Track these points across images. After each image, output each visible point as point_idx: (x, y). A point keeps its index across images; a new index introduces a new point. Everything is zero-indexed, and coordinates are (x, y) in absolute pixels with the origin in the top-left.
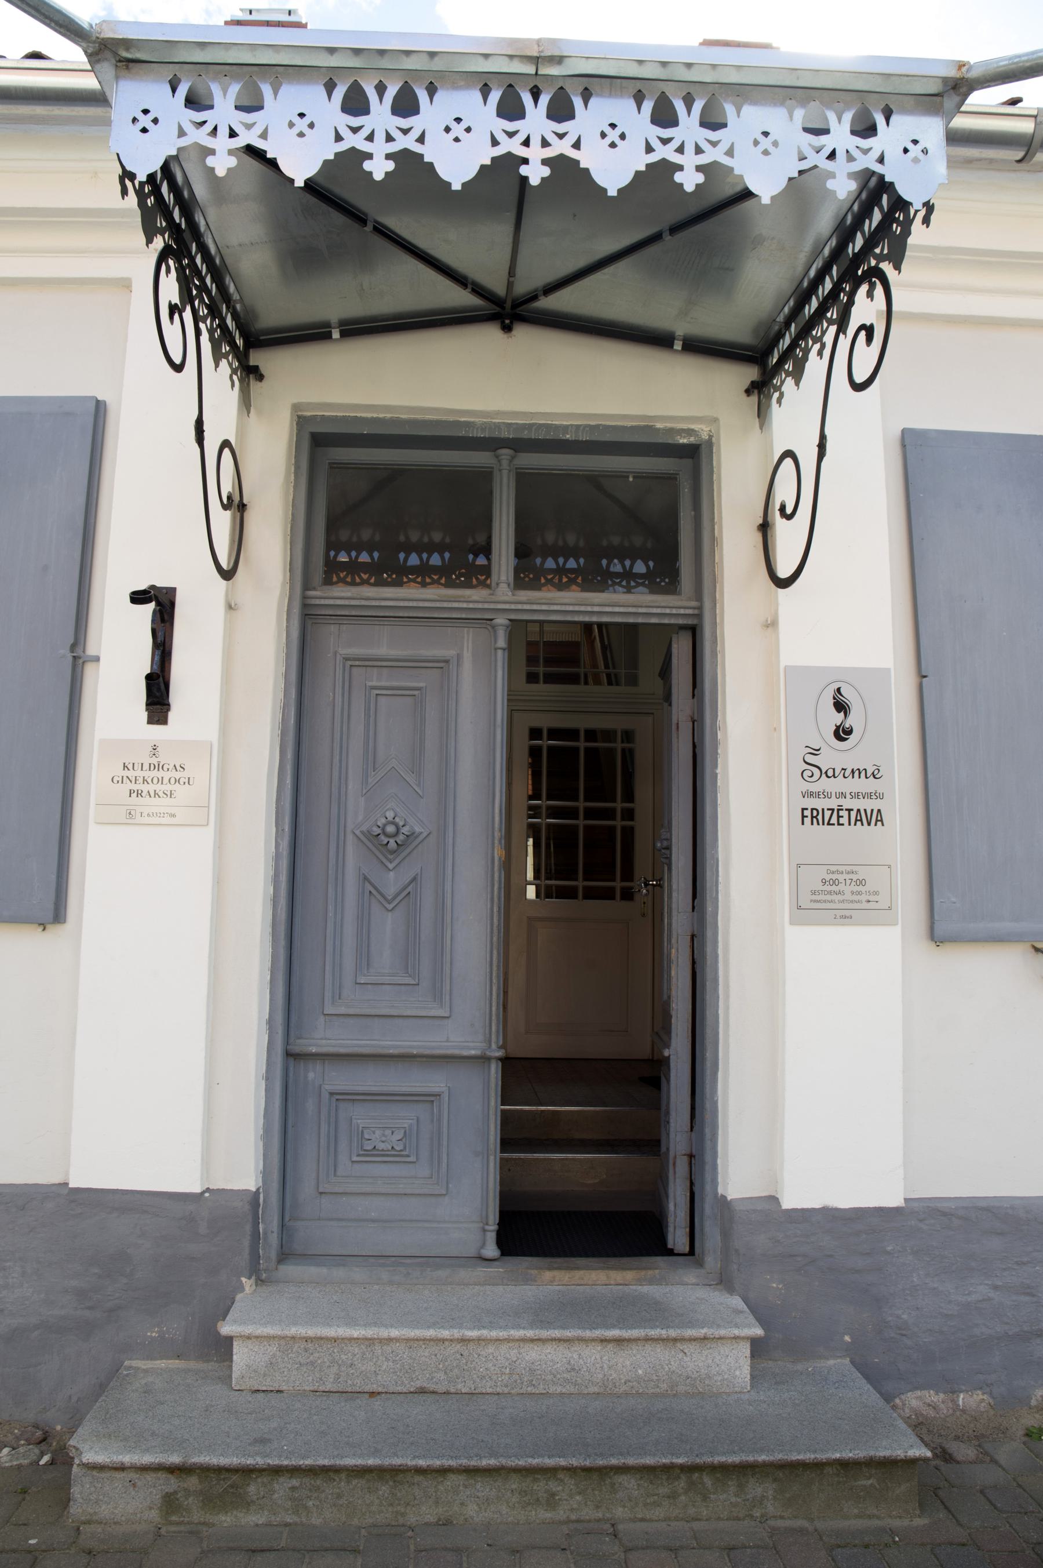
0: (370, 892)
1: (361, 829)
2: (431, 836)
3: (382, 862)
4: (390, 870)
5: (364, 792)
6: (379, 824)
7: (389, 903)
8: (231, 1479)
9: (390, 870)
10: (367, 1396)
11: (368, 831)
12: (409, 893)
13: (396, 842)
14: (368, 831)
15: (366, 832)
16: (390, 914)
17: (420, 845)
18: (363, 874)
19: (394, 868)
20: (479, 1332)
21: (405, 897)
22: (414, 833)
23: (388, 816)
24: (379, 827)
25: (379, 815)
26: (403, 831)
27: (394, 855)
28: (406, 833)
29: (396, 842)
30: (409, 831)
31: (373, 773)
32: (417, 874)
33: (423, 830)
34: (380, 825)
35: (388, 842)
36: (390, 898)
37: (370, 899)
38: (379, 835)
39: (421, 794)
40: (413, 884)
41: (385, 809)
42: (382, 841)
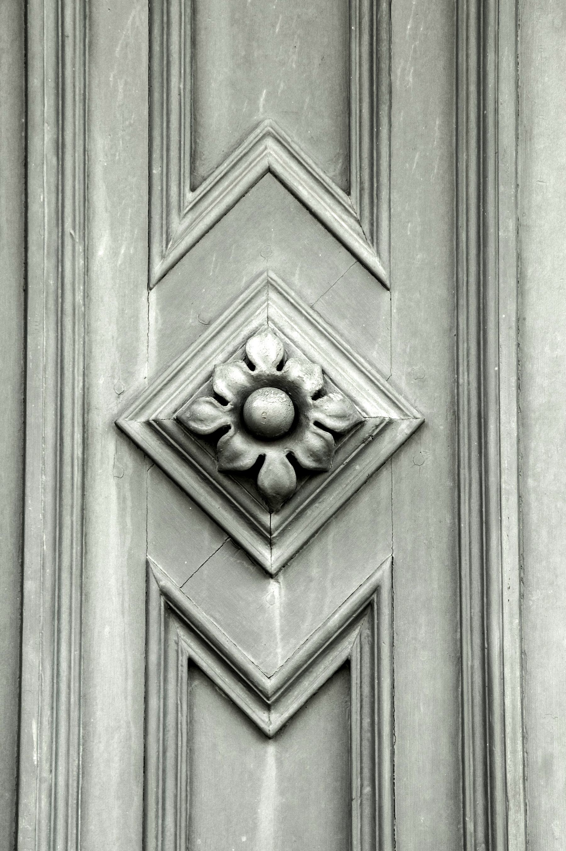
0: (192, 665)
1: (150, 414)
2: (426, 436)
3: (236, 545)
4: (267, 574)
5: (158, 268)
6: (221, 387)
7: (268, 707)
8: (286, 636)
9: (267, 574)
10: (176, 648)
11: (179, 421)
12: (346, 666)
13: (291, 457)
14: (179, 421)
15: (169, 424)
16: (271, 749)
17: (385, 474)
18: (164, 593)
19: (285, 565)
20: (64, 702)
21: (330, 681)
22: (359, 425)
23: (255, 357)
24: (222, 401)
25: (221, 357)
26: (315, 415)
27: (286, 512)
28: (330, 423)
29: (291, 457)
30: (341, 417)
31: (190, 197)
32: (376, 590)
33: (394, 415)
34: (229, 395)
35: (261, 459)
36: (269, 684)
37: (190, 694)
38: (224, 429)
39: (382, 272)
40: (362, 628)
41: (246, 331)
42: (236, 456)
